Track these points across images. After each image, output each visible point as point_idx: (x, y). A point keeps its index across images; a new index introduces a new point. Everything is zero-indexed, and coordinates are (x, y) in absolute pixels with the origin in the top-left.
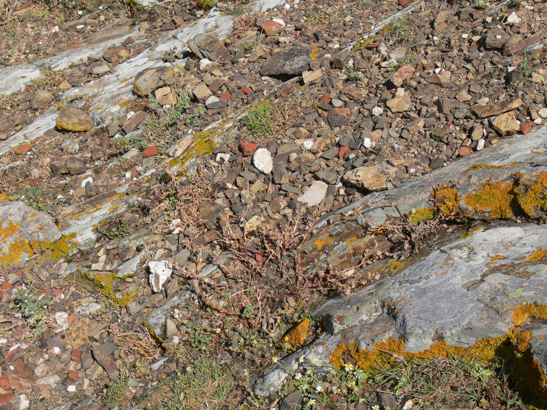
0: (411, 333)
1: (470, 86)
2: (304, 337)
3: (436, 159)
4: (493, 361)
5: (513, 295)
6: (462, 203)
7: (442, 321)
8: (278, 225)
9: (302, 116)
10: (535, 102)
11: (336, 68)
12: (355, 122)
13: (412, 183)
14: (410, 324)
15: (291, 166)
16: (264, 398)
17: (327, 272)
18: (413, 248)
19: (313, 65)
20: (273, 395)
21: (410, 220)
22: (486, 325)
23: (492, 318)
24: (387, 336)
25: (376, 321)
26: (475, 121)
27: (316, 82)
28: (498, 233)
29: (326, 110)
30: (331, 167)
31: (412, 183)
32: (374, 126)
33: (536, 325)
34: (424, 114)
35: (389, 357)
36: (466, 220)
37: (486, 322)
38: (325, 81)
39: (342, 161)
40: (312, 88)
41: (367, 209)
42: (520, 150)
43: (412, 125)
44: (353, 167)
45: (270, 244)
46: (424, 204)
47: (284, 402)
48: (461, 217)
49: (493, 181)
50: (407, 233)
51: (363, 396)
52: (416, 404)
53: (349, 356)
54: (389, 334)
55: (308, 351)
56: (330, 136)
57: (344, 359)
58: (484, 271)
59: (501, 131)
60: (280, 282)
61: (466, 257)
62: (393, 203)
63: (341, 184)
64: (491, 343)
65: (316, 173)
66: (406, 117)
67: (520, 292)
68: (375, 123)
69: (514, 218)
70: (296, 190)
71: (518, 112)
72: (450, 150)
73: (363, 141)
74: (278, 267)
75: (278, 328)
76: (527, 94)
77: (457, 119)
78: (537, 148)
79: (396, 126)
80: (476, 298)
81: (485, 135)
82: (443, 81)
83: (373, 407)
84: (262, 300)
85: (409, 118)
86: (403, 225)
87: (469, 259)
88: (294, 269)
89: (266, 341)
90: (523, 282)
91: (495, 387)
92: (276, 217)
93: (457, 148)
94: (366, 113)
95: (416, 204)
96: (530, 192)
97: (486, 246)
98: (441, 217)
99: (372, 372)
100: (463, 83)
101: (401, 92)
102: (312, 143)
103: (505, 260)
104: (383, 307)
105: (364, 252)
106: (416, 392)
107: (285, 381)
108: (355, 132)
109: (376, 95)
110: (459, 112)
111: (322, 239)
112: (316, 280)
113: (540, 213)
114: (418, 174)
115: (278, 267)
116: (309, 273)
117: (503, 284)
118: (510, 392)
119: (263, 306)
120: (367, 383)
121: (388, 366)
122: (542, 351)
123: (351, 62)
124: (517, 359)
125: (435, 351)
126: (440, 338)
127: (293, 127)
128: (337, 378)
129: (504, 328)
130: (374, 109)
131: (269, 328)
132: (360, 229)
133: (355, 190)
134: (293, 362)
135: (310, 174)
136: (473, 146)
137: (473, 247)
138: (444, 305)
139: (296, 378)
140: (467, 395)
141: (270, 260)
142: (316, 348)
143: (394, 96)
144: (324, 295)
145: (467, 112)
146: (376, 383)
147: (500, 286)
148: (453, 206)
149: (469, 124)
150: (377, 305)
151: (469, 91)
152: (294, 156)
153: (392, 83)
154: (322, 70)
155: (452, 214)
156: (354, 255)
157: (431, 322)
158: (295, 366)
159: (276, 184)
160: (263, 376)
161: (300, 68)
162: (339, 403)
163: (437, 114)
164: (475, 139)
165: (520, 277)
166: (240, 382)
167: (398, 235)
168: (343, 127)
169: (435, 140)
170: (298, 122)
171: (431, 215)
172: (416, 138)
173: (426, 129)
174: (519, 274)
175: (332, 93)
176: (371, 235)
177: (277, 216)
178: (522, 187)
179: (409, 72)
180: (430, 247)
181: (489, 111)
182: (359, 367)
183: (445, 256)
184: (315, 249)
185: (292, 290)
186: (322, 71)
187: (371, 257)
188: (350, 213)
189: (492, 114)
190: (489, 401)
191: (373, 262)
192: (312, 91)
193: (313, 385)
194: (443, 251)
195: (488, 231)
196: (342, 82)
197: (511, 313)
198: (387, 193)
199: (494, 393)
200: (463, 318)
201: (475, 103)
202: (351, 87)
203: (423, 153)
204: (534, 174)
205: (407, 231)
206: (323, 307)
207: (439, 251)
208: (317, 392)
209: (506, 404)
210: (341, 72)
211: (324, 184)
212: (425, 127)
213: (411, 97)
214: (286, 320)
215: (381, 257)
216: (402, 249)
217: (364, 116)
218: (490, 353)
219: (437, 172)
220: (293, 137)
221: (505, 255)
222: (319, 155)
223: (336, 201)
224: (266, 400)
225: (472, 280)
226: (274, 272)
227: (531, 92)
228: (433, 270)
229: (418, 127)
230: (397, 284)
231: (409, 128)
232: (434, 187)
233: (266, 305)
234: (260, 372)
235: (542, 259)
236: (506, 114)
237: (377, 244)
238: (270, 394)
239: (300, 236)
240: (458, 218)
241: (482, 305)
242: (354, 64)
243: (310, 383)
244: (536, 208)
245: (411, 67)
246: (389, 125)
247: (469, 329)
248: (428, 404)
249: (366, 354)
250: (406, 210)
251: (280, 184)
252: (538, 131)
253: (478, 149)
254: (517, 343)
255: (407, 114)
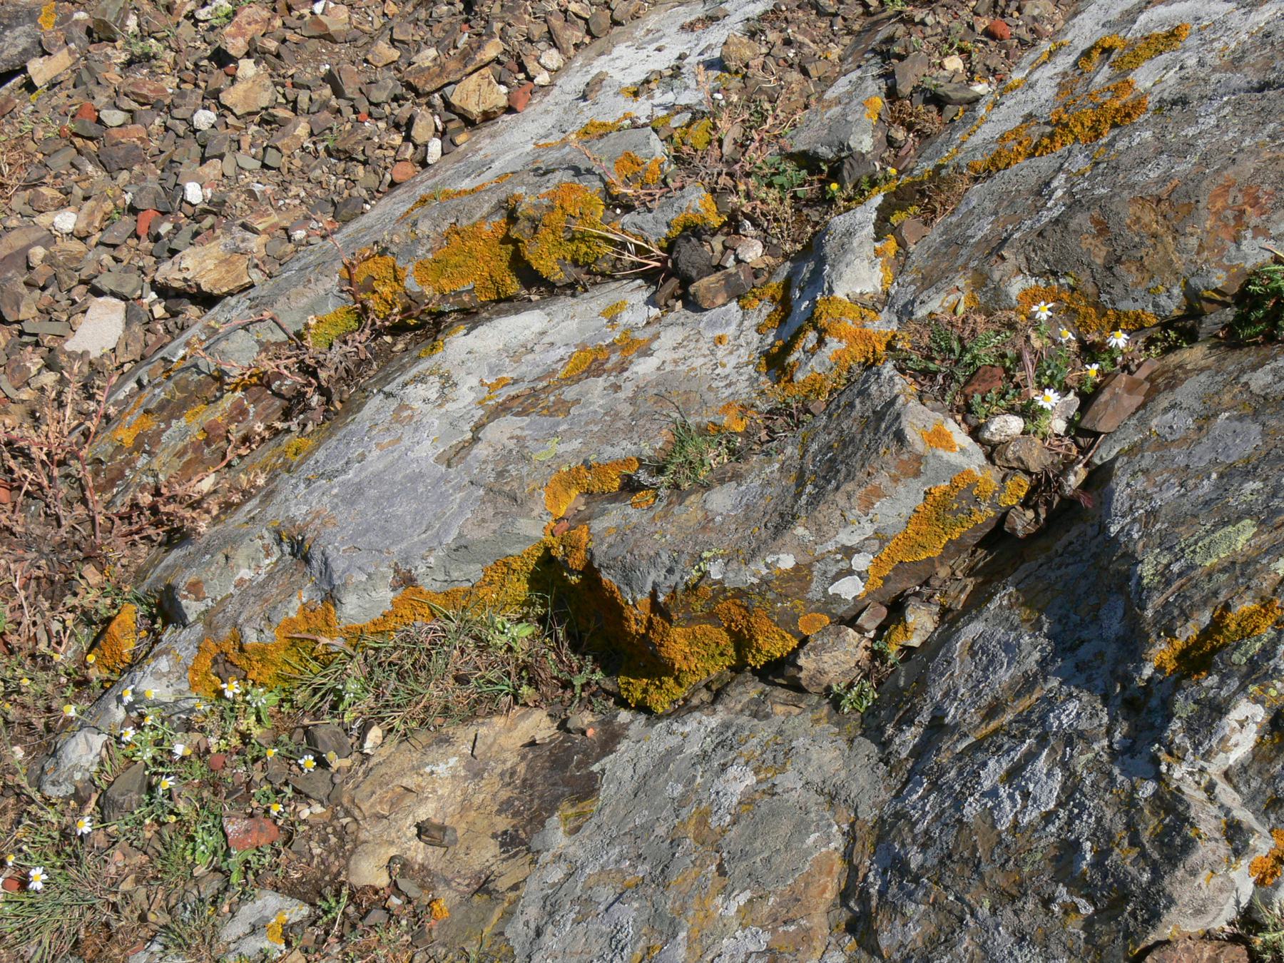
0: (345, 585)
1: (391, 29)
2: (129, 646)
3: (346, 200)
4: (529, 603)
5: (540, 456)
6: (411, 284)
7: (404, 545)
8: (32, 414)
9: (40, 162)
10: (529, 40)
11: (100, 40)
12: (161, 152)
13: (303, 262)
14: (338, 565)
15: (36, 277)
16: (66, 800)
17: (157, 492)
18: (329, 401)
19: (49, 43)
20: (85, 788)
21: (309, 342)
22: (494, 532)
23: (505, 515)
24: (296, 603)
25: (271, 576)
26: (414, 103)
27: (62, 78)
28: (496, 332)
29: (91, 139)
30: (125, 263)
31: (303, 262)
32: (203, 154)
33: (597, 507)
34: (306, 107)
35: (311, 645)
36: (428, 318)
37: (495, 526)
38: (79, 75)
39: (146, 244)
40: (55, 94)
41: (216, 337)
42: (512, 148)
43: (284, 135)
44: (173, 252)
45: (21, 459)
46: (331, 301)
47: (109, 799)
48: (416, 313)
49: (465, 222)
50: (309, 371)
51: (276, 743)
52: (391, 730)
53: (227, 665)
54: (300, 598)
55: (139, 674)
56: (110, 193)
57: (218, 675)
58: (476, 419)
59: (471, 113)
60: (58, 538)
61: (436, 396)
62: (265, 313)
63: (153, 295)
64: (515, 566)
65: (94, 281)
66: (268, 121)
67: (554, 447)
68: (204, 147)
69: (524, 292)
70: (57, 328)
71: (499, 68)
72: (373, 175)
73: (184, 190)
74: (47, 506)
75: (73, 639)
76: (510, 25)
77: (377, 105)
78: (546, 137)
79: (252, 145)
80: (468, 479)
81: (440, 128)
82: (332, 28)
83: (300, 762)
84: (25, 587)
85: (275, 122)
86: (297, 356)
87: (443, 397)
88: (84, 501)
89: (51, 673)
90: (558, 424)
91: (544, 655)
92: (24, 397)
93: (386, 168)
94: (181, 128)
95: (314, 304)
96: (543, 231)
97: (474, 365)
98: (374, 323)
99: (287, 686)
100: (377, 24)
101: (247, 68)
102: (74, 216)
103: (516, 386)
104: (280, 541)
105: (228, 431)
106: (386, 706)
107: (104, 752)
108: (165, 175)
109: (196, 85)
110: (379, 89)
111: (129, 424)
112: (135, 514)
113: (574, 272)
114: (312, 240)
115: (47, 506)
116: (118, 503)
117: (518, 438)
118: (575, 660)
119: (31, 599)
120: (280, 712)
121: (315, 666)
122: (615, 559)
123: (132, 23)
124: (573, 588)
125: (404, 612)
126: (406, 581)
127: (25, 188)
128: (216, 717)
129: (533, 529)
130: (195, 117)
131: (53, 644)
132: (207, 384)
133: (185, 301)
134: (113, 706)
135: (82, 287)
136: (419, 157)
137: (448, 371)
138: (403, 508)
139: (123, 739)
140: (492, 687)
141: (27, 494)
142: (153, 664)
143: (234, 79)
144: (160, 545)
145: (395, 86)
146: (299, 709)
147: (511, 444)
148: (394, 293)
149: (403, 112)
150: (266, 542)
151: (392, 41)
152: (38, 253)
153: (225, 52)
154: (69, 50)
155: (396, 310)
156: (208, 442)
157: (380, 551)
158: (120, 714)
159: (10, 323)
160: (54, 754)
161: (20, 53)
162: (228, 771)
163: (334, 102)
164: (419, 141)
165: (551, 416)
166: (9, 777)
167: (292, 380)
168: (137, 168)
169: (340, 160)
170: (34, 176)
171: (352, 323)
172: (297, 162)
173: (314, 139)
174: (548, 408)
175: (97, 98)
176: (234, 390)
177: (25, 394)
178: (526, 223)
179: (257, 22)
180: (364, 390)
181: (439, 75)
182: (254, 685)
183: (393, 404)
184: (119, 449)
185: (88, 549)
186: (71, 52)
187: (246, 440)
188: (181, 353)
189: (446, 81)
190: (537, 689)
191: (252, 450)
192: (54, 102)
193: (166, 744)
194: (389, 395)
195: (475, 332)
196: (117, 69)
197: (540, 495)
198: (252, 293)
199: (543, 670)
200: (446, 527)
201: (410, 64)
202: (139, 76)
203: (318, 192)
204: (543, 191)
205: (309, 366)
206: (158, 570)
207: (381, 396)
208: (177, 758)
209: (573, 687)
210: (115, 47)
211: (116, 301)
212: (311, 134)
213: (271, 76)
214: (87, 618)
215: (267, 434)
216: (307, 408)
217: (178, 136)
218: (520, 588)
219: (352, 227)
220: (29, 210)
221: (514, 375)
222: (93, 240)
223: (149, 335)
224: (72, 802)
225: (454, 442)
226: (42, 519)
227: (518, 19)
228: (371, 439)
229: (298, 137)
230: (302, 486)
231: (279, 144)
232: (345, 261)
233: (36, 594)
234: (49, 744)
235: (589, 367)
236: (475, 75)
237: (252, 409)
238: (76, 789)
239: (82, 428)
240: (410, 317)
241: (482, 492)
242: (139, 25)
243: (158, 743)
244: (561, 262)
245: (260, 10)
246: (235, 146)
247: (462, 549)
248: (414, 725)
249: (262, 651)
250: (296, 323)
251: (19, 322)
252: (545, 100)
253: (430, 160)
254: (566, 555)
255: (269, 114)
